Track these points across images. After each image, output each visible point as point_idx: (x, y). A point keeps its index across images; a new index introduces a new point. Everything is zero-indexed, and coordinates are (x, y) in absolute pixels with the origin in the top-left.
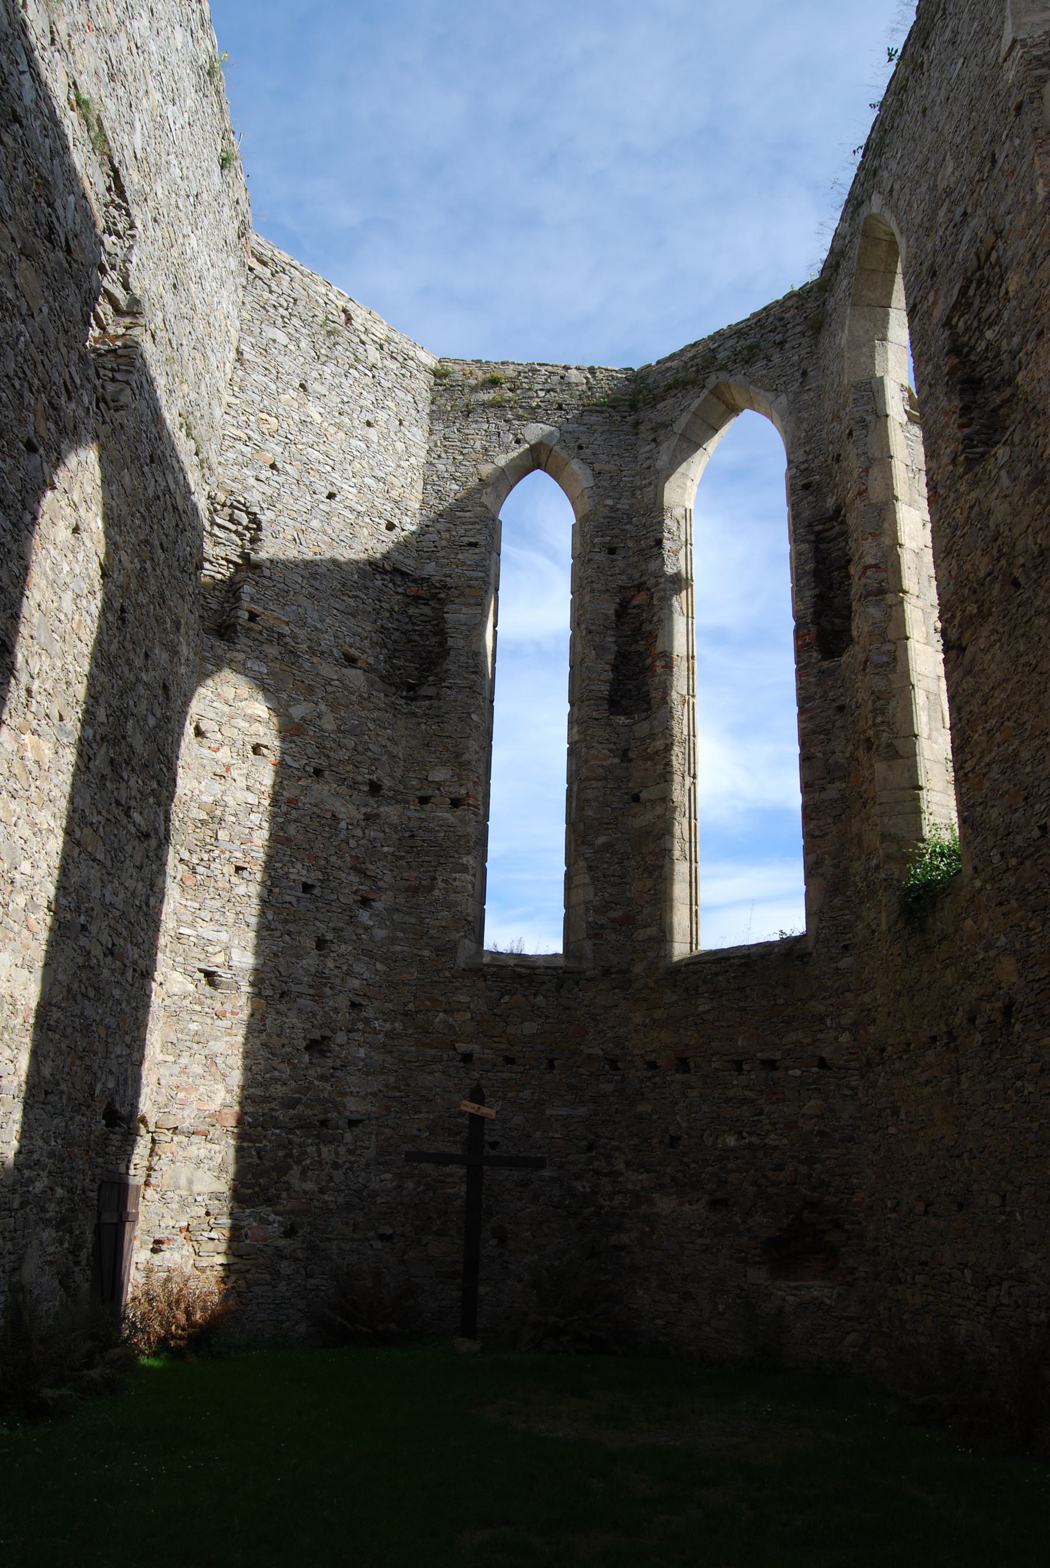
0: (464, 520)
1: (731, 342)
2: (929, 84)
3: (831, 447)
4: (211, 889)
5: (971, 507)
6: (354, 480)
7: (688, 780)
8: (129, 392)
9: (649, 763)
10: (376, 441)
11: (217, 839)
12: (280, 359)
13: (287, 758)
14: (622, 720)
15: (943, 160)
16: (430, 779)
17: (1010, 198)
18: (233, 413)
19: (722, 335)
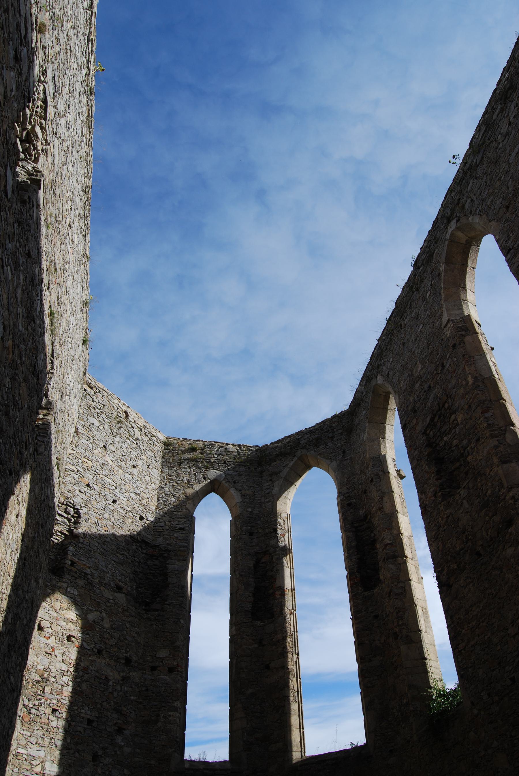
0: (178, 516)
1: (307, 436)
2: (405, 333)
3: (360, 486)
4: (38, 723)
5: (448, 517)
6: (125, 494)
7: (295, 656)
8: (43, 446)
9: (274, 647)
10: (137, 475)
11: (44, 692)
12: (95, 433)
13: (85, 644)
14: (259, 623)
15: (416, 364)
16: (157, 656)
17: (454, 382)
18: (71, 458)
19: (302, 432)
